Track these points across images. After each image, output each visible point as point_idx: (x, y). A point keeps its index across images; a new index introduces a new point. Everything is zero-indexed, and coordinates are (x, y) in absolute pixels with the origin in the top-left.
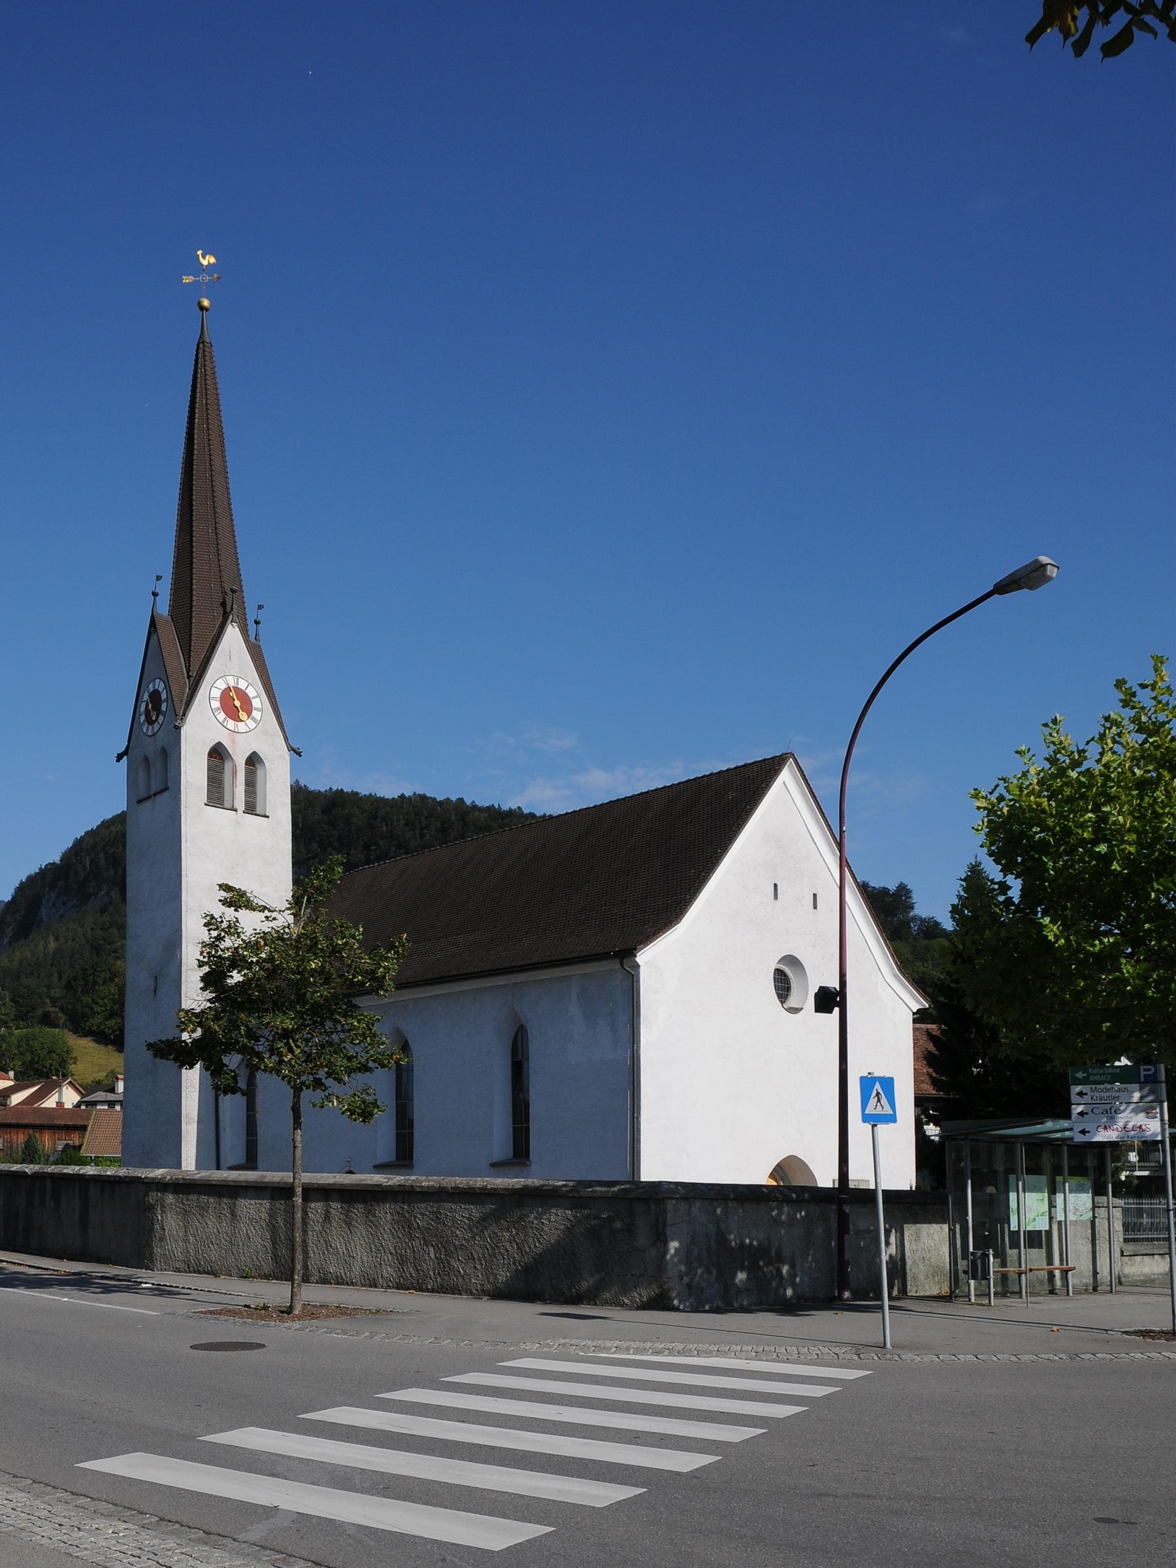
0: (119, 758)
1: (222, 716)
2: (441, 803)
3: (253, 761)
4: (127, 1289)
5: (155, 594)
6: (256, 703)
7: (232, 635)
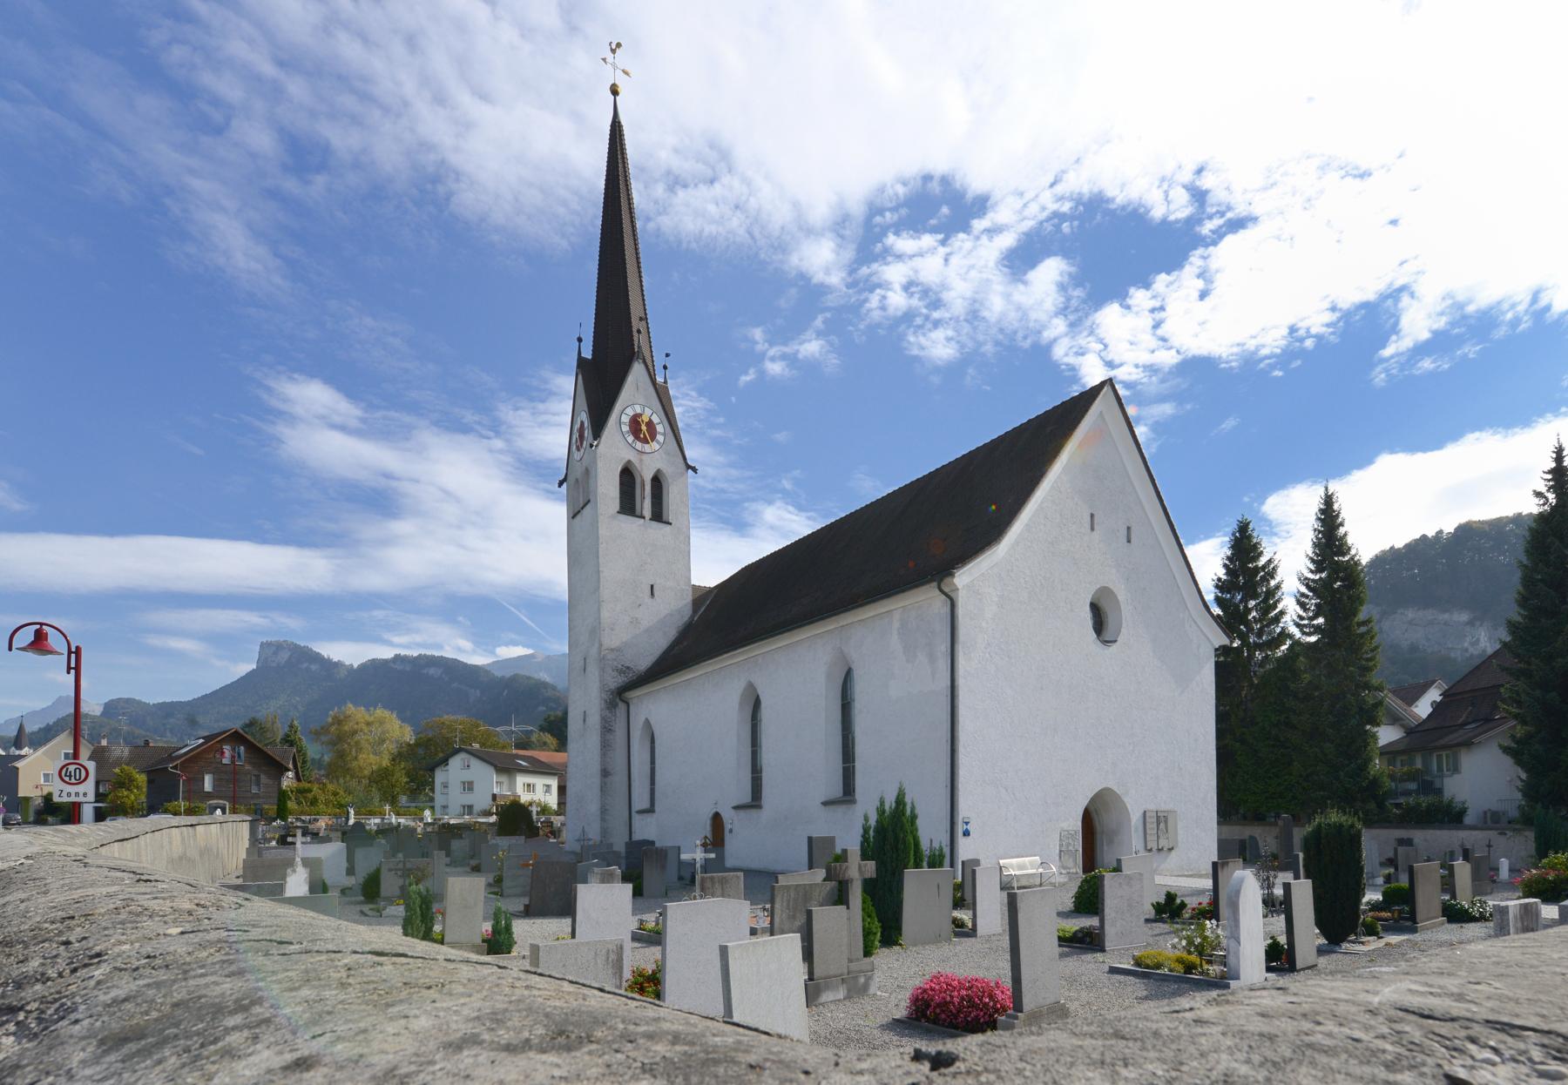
0: (560, 484)
1: (630, 439)
2: (1286, 356)
3: (657, 481)
4: (866, 947)
5: (580, 340)
6: (660, 428)
7: (637, 371)
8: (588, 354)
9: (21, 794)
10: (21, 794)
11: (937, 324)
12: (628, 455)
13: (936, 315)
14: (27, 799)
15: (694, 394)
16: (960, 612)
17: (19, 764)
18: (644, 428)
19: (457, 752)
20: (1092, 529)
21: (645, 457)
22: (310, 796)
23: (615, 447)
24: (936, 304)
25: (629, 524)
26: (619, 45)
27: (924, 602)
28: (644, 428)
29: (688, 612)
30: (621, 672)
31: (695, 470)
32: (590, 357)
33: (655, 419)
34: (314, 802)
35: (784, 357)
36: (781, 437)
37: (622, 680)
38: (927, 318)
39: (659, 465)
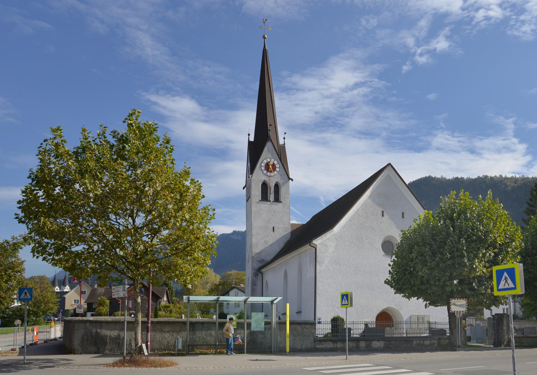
1: (265, 172)
3: (277, 186)
5: (249, 135)
6: (277, 166)
7: (269, 145)
8: (252, 139)
9: (66, 309)
10: (66, 309)
11: (523, 22)
12: (264, 178)
13: (522, 17)
14: (68, 310)
15: (376, 80)
16: (318, 252)
17: (66, 296)
18: (271, 167)
19: (233, 288)
20: (383, 216)
21: (271, 178)
22: (169, 309)
23: (259, 176)
24: (523, 11)
25: (265, 206)
26: (266, 20)
27: (307, 247)
28: (271, 167)
29: (289, 237)
30: (260, 262)
31: (292, 180)
32: (253, 140)
33: (276, 162)
34: (171, 312)
35: (428, 52)
36: (432, 96)
37: (260, 265)
38: (517, 21)
39: (277, 180)
